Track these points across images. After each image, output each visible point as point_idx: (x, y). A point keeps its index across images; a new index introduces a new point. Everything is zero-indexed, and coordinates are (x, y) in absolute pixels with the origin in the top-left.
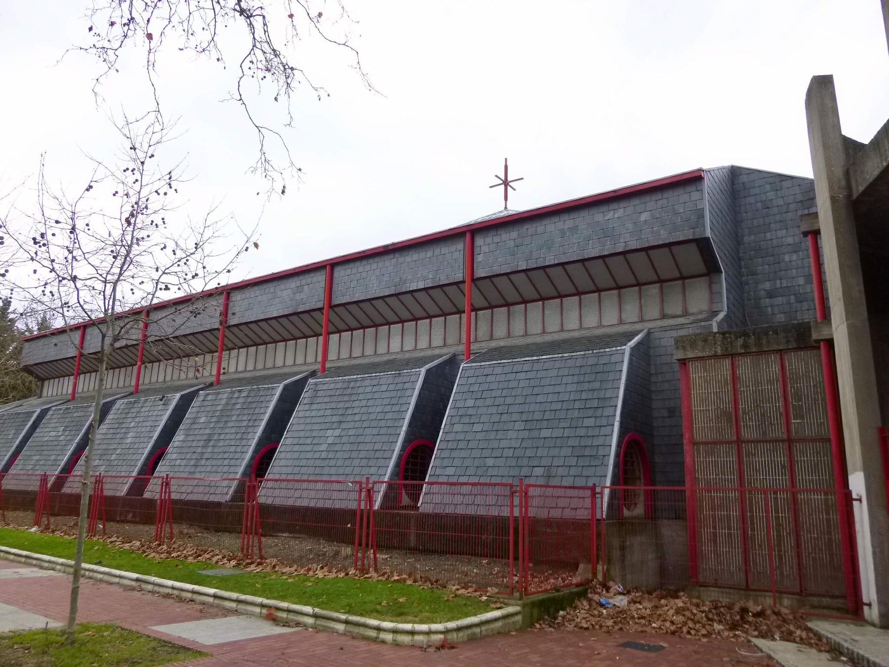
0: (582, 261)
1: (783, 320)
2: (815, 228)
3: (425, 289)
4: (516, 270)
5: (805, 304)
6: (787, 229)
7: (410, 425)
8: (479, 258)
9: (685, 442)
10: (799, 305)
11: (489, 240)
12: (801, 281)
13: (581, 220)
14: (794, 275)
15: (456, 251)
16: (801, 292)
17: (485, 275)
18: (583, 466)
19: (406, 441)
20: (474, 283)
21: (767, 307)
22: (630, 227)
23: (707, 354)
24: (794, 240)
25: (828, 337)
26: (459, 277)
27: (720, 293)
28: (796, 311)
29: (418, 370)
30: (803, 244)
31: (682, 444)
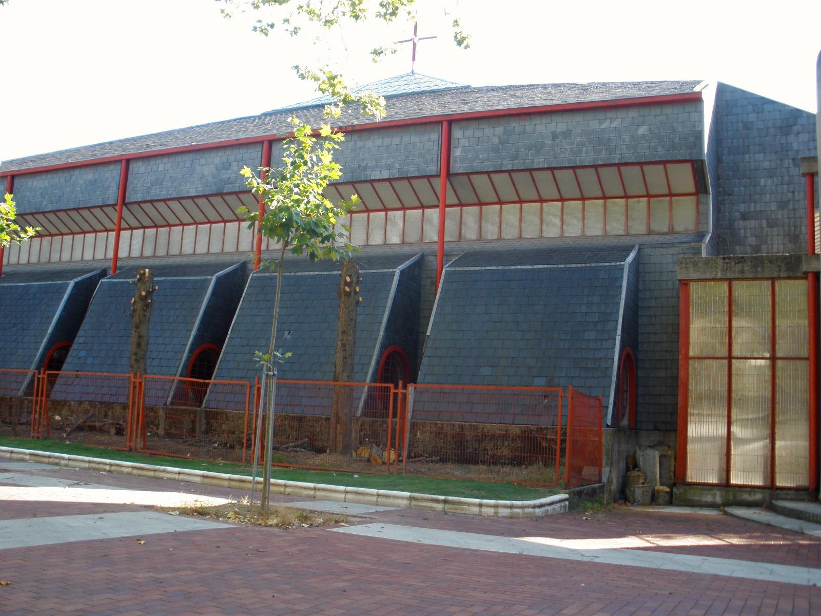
0: (573, 168)
1: (754, 244)
2: (814, 171)
3: (389, 180)
4: (500, 169)
5: (775, 229)
6: (765, 153)
7: (387, 329)
8: (457, 152)
9: (680, 357)
10: (769, 230)
11: (469, 133)
12: (774, 207)
13: (576, 122)
14: (768, 200)
15: (431, 140)
16: (773, 217)
17: (464, 172)
18: (586, 377)
19: (383, 346)
20: (449, 179)
21: (740, 229)
22: (627, 140)
23: (708, 276)
24: (770, 165)
25: (815, 270)
26: (432, 169)
27: (707, 214)
28: (767, 236)
29: (391, 270)
30: (778, 170)
31: (678, 360)
